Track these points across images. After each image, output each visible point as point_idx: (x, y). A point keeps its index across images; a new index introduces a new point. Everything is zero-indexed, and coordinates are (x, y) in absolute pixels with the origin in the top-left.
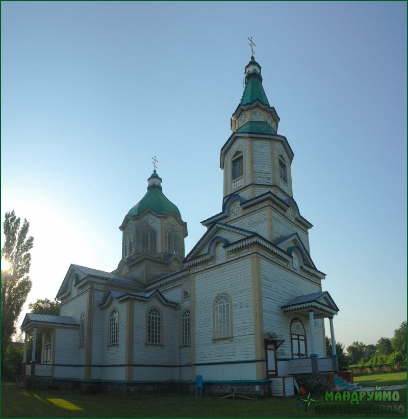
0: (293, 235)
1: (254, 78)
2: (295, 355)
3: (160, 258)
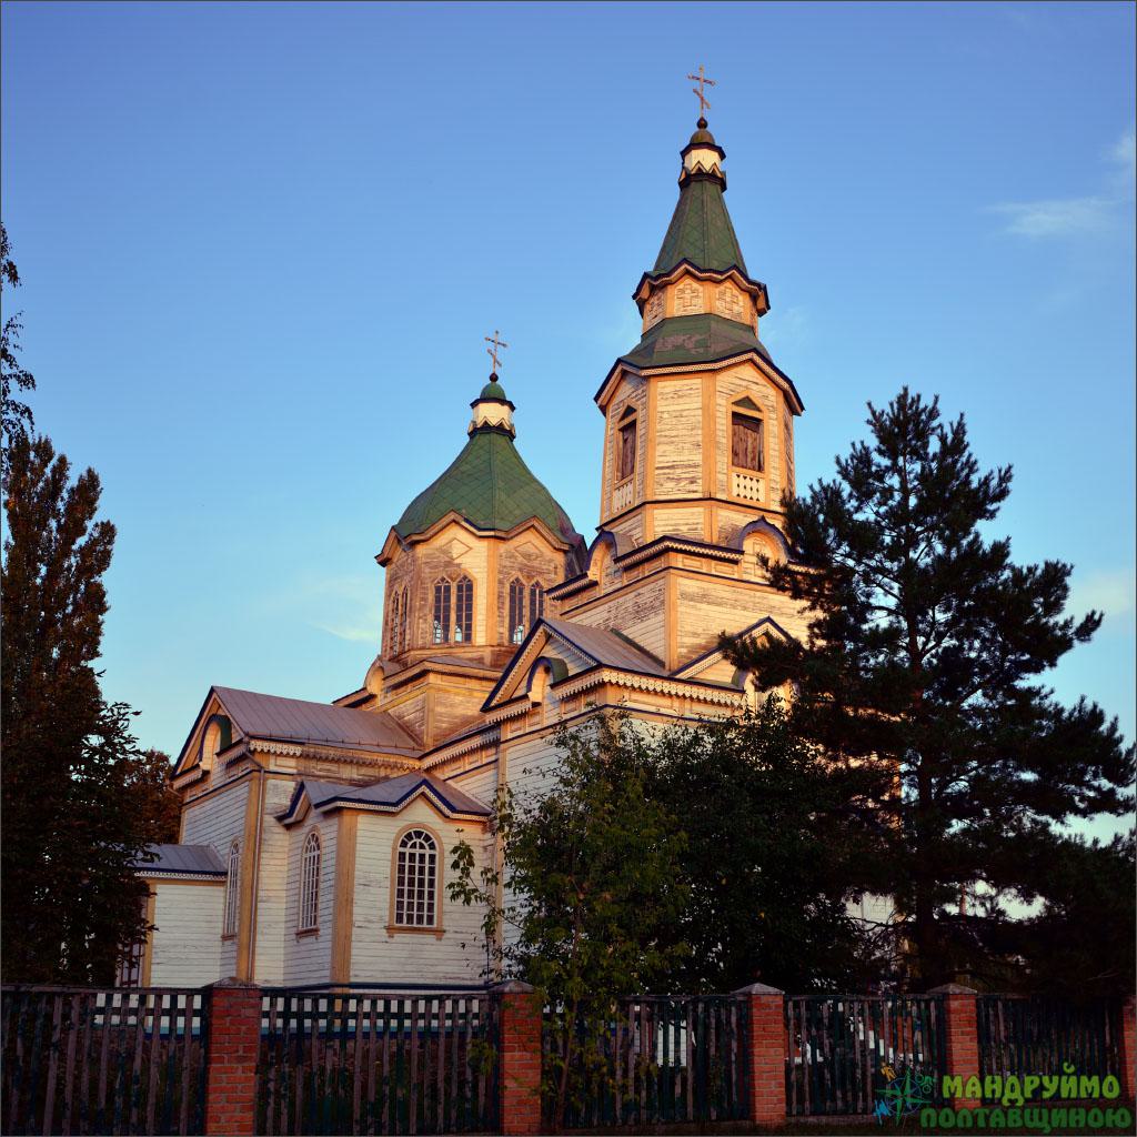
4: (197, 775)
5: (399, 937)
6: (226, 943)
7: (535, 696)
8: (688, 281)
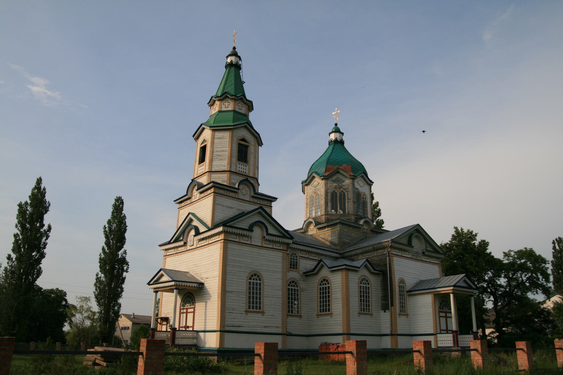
3: (350, 219)
5: (249, 314)
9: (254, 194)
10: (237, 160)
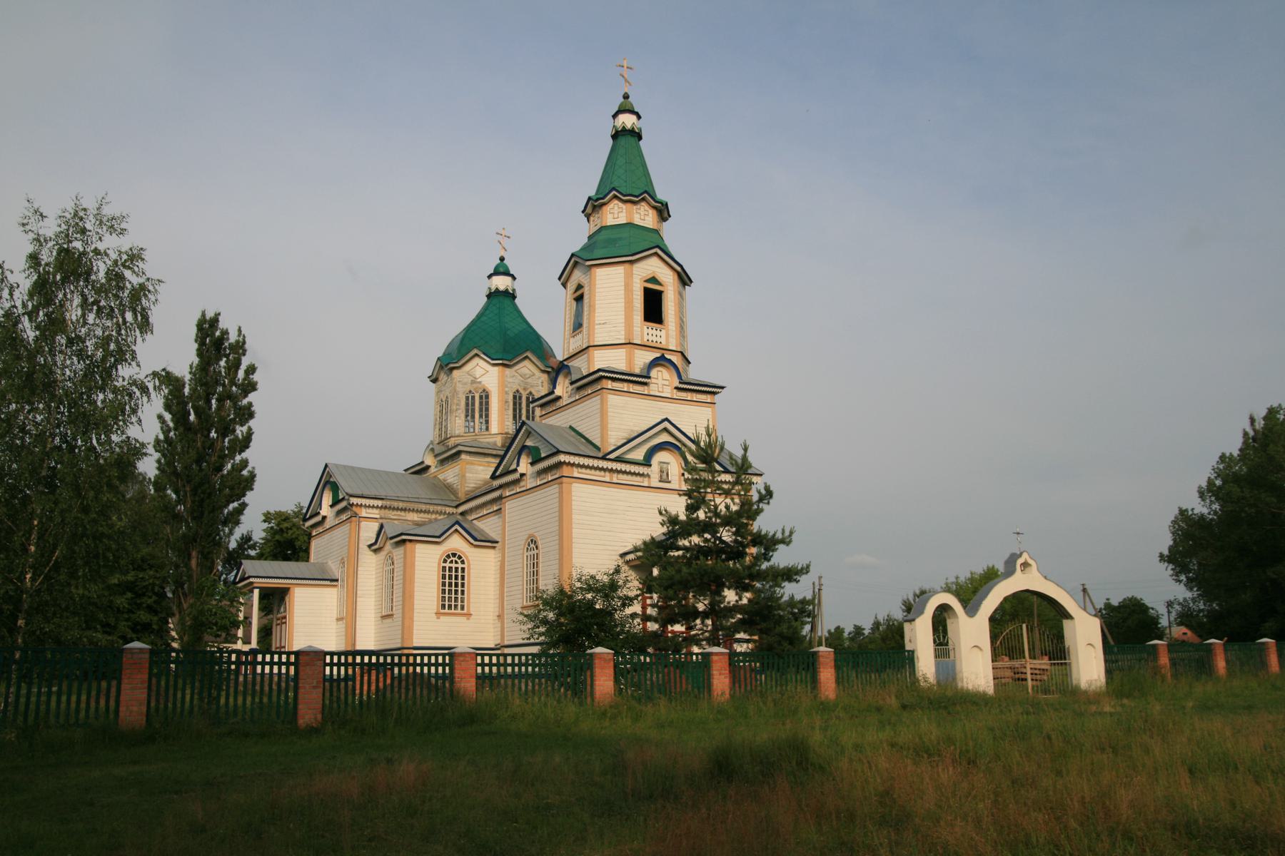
0: (663, 421)
1: (626, 138)
2: (808, 622)
4: (318, 518)
5: (443, 618)
6: (339, 623)
7: (522, 469)
8: (616, 202)
9: (680, 383)
10: (643, 319)
